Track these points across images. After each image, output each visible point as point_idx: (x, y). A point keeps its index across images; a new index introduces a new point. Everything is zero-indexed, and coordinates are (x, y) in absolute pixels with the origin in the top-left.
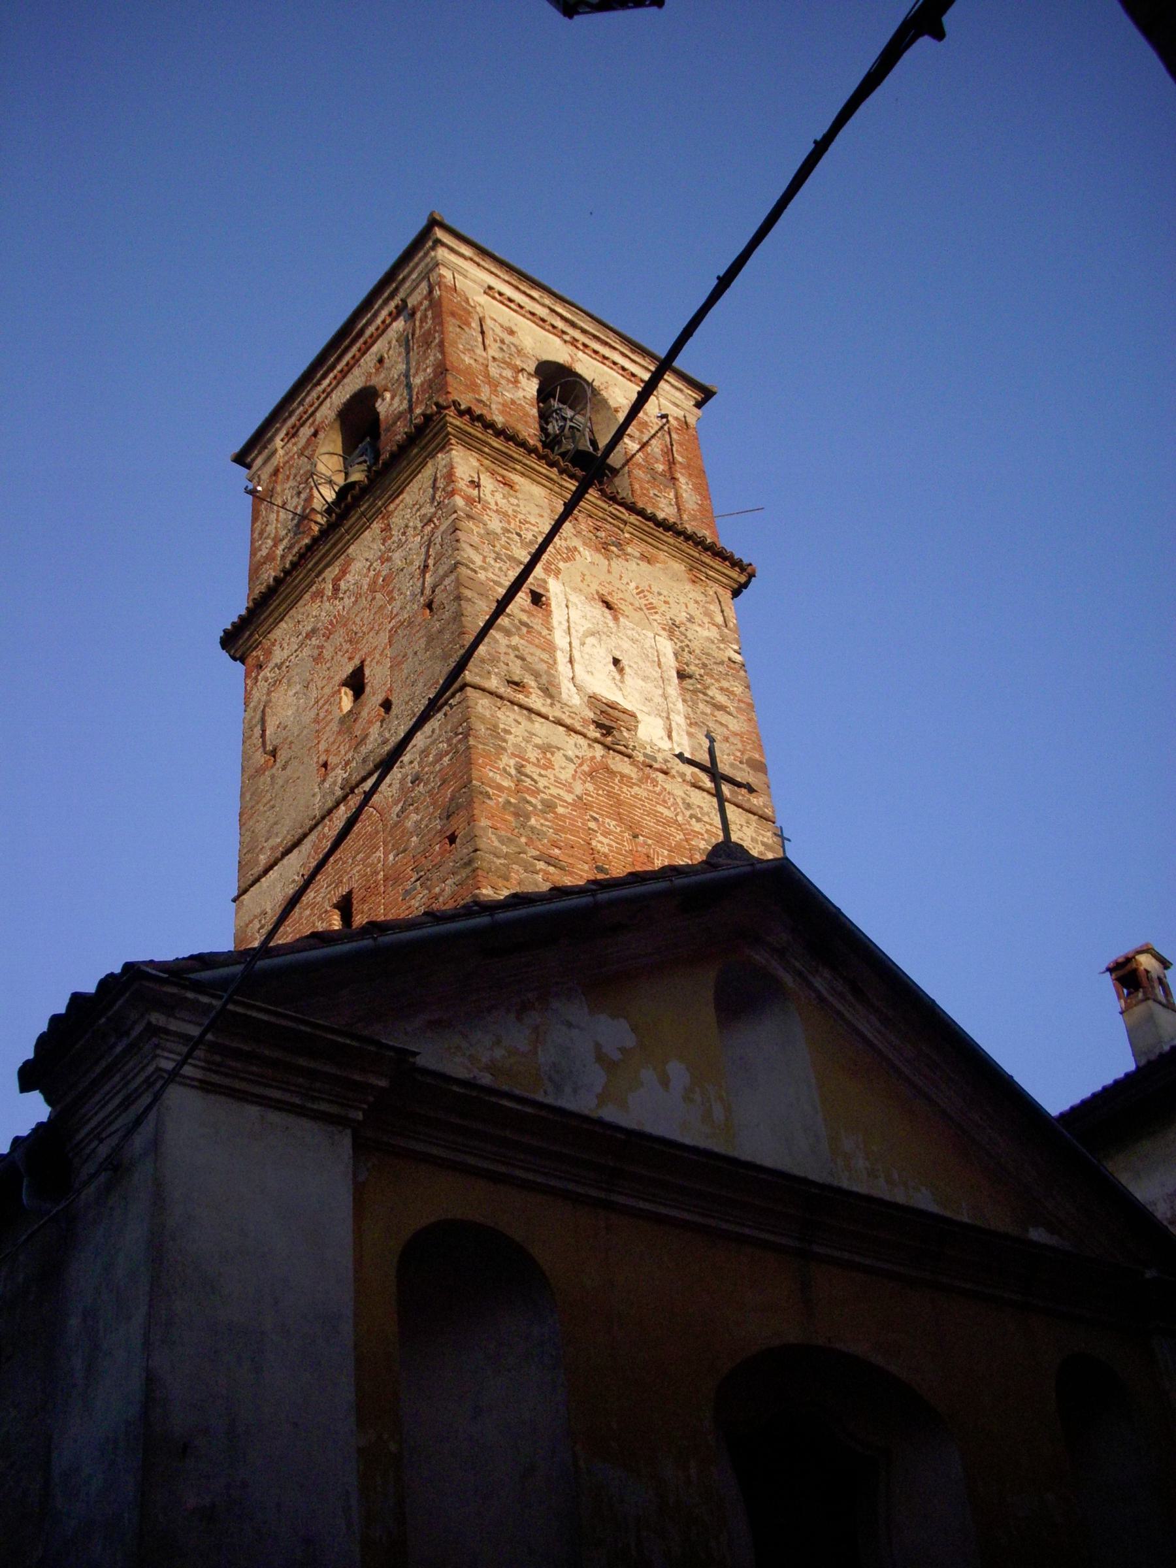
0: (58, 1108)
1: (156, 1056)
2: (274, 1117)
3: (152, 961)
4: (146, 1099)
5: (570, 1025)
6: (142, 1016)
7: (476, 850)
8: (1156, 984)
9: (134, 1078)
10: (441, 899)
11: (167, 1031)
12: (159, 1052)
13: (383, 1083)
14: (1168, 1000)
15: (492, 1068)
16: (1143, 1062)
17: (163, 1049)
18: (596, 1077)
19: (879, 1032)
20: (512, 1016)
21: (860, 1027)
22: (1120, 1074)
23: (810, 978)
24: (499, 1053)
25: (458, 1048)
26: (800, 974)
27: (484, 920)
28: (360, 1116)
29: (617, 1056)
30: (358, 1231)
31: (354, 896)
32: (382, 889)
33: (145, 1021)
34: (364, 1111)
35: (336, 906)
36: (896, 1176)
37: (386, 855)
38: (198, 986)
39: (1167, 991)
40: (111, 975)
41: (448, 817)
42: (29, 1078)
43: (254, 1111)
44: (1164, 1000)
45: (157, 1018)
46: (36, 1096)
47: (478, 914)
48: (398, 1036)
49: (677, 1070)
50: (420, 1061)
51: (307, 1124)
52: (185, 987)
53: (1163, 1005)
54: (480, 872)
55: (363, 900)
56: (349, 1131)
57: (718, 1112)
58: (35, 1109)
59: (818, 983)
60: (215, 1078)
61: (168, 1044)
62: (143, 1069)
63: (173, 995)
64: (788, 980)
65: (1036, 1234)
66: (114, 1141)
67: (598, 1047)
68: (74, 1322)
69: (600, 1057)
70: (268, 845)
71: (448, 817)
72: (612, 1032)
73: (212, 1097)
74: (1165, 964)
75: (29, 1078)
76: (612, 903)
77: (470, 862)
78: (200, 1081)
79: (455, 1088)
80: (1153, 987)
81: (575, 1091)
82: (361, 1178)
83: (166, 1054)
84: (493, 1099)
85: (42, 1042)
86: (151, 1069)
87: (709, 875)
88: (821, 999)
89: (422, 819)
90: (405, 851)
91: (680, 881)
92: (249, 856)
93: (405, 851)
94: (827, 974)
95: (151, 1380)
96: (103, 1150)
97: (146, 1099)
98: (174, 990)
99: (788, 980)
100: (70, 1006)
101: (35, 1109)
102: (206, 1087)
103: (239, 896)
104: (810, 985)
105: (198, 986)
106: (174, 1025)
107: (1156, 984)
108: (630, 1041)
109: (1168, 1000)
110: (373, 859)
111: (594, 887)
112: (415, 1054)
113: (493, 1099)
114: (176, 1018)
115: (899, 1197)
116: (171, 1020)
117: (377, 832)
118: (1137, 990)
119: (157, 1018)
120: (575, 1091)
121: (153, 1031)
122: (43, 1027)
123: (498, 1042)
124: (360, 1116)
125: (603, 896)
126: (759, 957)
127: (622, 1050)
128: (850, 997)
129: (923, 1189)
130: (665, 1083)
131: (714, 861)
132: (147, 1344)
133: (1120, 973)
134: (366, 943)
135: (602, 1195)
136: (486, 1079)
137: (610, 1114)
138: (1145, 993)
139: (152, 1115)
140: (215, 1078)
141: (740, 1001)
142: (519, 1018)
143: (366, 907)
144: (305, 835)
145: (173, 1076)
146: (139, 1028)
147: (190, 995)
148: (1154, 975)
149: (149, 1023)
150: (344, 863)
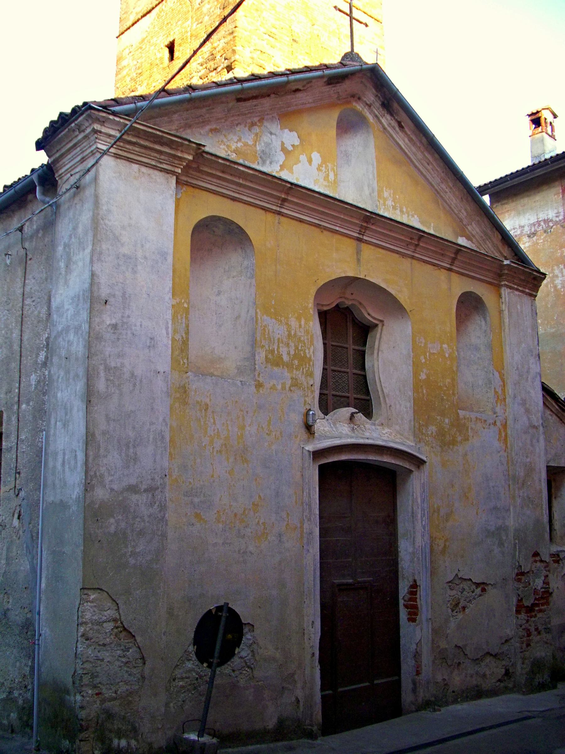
0: (52, 159)
1: (96, 142)
2: (144, 169)
3: (95, 102)
4: (91, 162)
5: (271, 133)
6: (90, 125)
7: (236, 27)
8: (548, 125)
9: (86, 150)
10: (217, 49)
11: (100, 132)
12: (97, 141)
13: (190, 158)
14: (552, 134)
15: (236, 151)
16: (536, 162)
17: (99, 139)
18: (281, 158)
19: (408, 146)
20: (247, 128)
21: (400, 143)
22: (525, 166)
23: (381, 118)
24: (240, 145)
25: (222, 141)
26: (376, 116)
27: (238, 86)
28: (180, 171)
29: (290, 148)
30: (176, 219)
31: (176, 42)
32: (189, 40)
33: (92, 128)
34: (181, 169)
35: (167, 46)
36: (404, 210)
37: (192, 23)
38: (114, 114)
39: (553, 130)
40: (78, 106)
41: (224, 8)
42: (40, 145)
43: (135, 167)
44: (550, 134)
45: (97, 126)
46: (42, 152)
47: (236, 83)
48: (197, 136)
49: (316, 157)
50: (207, 149)
51: (157, 172)
52: (109, 114)
53: (549, 136)
54: (237, 38)
55: (180, 45)
56: (175, 177)
57: (332, 177)
58: (42, 158)
59: (383, 121)
60: (120, 152)
61: (101, 137)
62: (90, 147)
63: (104, 117)
64: (370, 118)
65: (462, 241)
66: (77, 176)
67: (283, 144)
68: (60, 248)
69: (284, 149)
70: (135, 11)
71: (224, 8)
72: (290, 138)
73: (119, 160)
74: (555, 116)
75: (40, 145)
76: (296, 81)
77: (232, 33)
78: (114, 154)
79: (220, 161)
80: (546, 126)
81: (271, 163)
82: (178, 197)
83: (100, 142)
84: (236, 166)
85: (46, 131)
86: (94, 147)
87: (340, 70)
88: (385, 129)
89: (211, 8)
90: (201, 22)
91: (327, 72)
92: (125, 16)
93: (201, 22)
94: (388, 117)
95: (93, 275)
96: (73, 180)
97: (91, 162)
98: (104, 115)
99: (370, 118)
100: (59, 118)
101: (42, 158)
102: (117, 156)
103: (119, 36)
104: (381, 123)
105: (114, 114)
106: (104, 130)
107: (548, 125)
108: (297, 142)
109: (552, 134)
110: (186, 24)
111: (288, 72)
112: (204, 146)
113: (236, 166)
114: (105, 126)
115: (405, 220)
116: (103, 127)
117: (188, 11)
118: (539, 127)
119: (97, 126)
120: (271, 163)
121: (95, 131)
122: (47, 125)
123: (240, 140)
124: (180, 171)
125: (292, 77)
126: (359, 107)
127: (293, 146)
128: (397, 129)
129: (416, 216)
130: (310, 161)
131: (344, 62)
132: (92, 262)
133: (533, 117)
134: (187, 95)
135: (278, 209)
136: (233, 157)
137: (285, 175)
138: (542, 129)
139: (94, 169)
140: (120, 152)
141: (347, 126)
142: (250, 130)
143: (181, 48)
144: (153, 8)
145: (105, 153)
146: (89, 130)
147: (111, 117)
148: (548, 121)
149: (94, 129)
150: (172, 25)
